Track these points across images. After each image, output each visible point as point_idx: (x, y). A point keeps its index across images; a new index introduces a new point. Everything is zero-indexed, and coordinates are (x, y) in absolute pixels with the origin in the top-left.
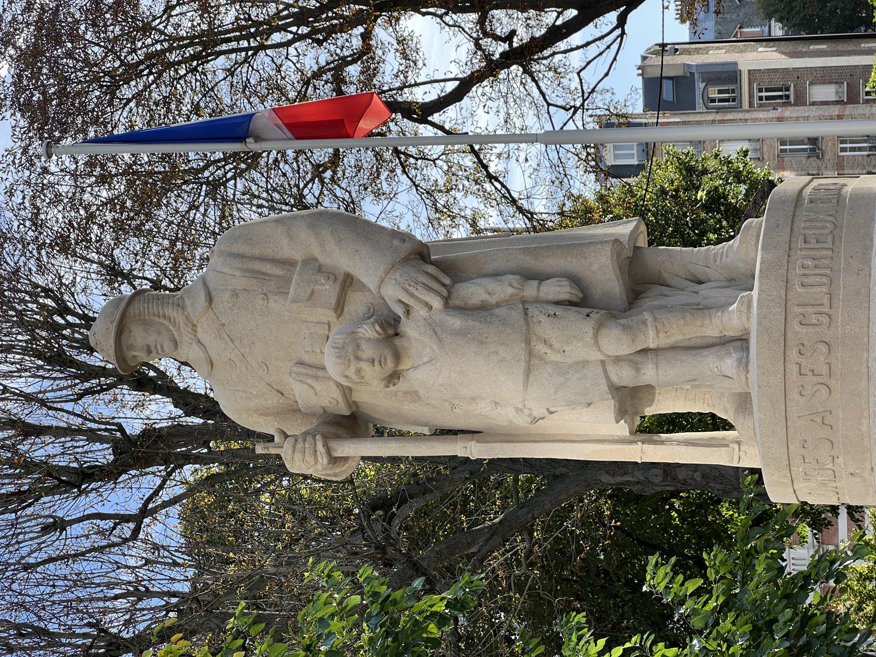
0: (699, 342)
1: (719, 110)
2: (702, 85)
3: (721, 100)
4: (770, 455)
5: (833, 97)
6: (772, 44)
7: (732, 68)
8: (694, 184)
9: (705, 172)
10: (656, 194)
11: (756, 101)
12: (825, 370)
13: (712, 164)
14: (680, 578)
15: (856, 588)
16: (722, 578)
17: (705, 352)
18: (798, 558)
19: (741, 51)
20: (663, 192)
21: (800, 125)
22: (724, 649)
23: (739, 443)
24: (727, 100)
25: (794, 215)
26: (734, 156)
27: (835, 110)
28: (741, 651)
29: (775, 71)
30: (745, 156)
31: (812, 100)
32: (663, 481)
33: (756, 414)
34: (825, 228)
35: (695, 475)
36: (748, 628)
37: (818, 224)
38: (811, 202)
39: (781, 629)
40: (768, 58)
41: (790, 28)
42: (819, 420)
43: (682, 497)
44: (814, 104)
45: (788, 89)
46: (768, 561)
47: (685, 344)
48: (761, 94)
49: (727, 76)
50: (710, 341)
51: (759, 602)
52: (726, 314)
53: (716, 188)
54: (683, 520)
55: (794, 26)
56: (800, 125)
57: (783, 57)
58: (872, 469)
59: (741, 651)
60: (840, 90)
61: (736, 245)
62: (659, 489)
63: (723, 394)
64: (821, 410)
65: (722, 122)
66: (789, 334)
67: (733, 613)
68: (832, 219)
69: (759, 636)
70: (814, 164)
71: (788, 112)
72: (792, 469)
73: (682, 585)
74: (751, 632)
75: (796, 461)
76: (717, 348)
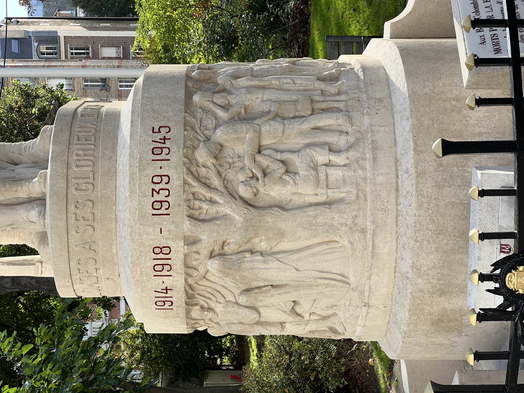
0: (15, 201)
1: (47, 60)
2: (36, 44)
3: (48, 54)
4: (59, 269)
5: (114, 55)
6: (78, 21)
7: (54, 35)
8: (30, 104)
9: (37, 97)
10: (7, 110)
11: (69, 55)
12: (91, 217)
13: (41, 92)
14: (19, 344)
15: (129, 343)
16: (44, 343)
17: (18, 207)
18: (93, 328)
19: (59, 25)
20: (11, 108)
21: (95, 71)
22: (45, 386)
23: (41, 262)
24: (52, 54)
25: (72, 124)
26: (54, 88)
27: (116, 63)
28: (55, 387)
29: (80, 37)
30: (62, 88)
31: (102, 56)
32: (11, 286)
33: (50, 244)
34: (90, 131)
35: (32, 281)
36: (59, 372)
37: (86, 129)
38: (82, 116)
39: (77, 372)
40: (76, 30)
41: (88, 12)
42: (88, 247)
43: (25, 295)
44: (103, 58)
45: (88, 49)
46: (73, 331)
47: (6, 202)
48: (72, 51)
49: (51, 39)
50: (22, 200)
51: (66, 357)
52: (31, 184)
53: (44, 107)
54: (26, 309)
55: (91, 11)
56: (95, 71)
57: (85, 29)
58: (119, 275)
59: (55, 387)
60: (119, 51)
61: (38, 141)
62: (9, 291)
63: (31, 233)
64: (89, 241)
65: (48, 66)
66: (69, 196)
67: (51, 364)
68: (94, 126)
69: (66, 377)
70: (105, 94)
71: (88, 63)
72: (72, 277)
73: (20, 348)
74: (61, 374)
75: (75, 272)
76: (26, 205)
